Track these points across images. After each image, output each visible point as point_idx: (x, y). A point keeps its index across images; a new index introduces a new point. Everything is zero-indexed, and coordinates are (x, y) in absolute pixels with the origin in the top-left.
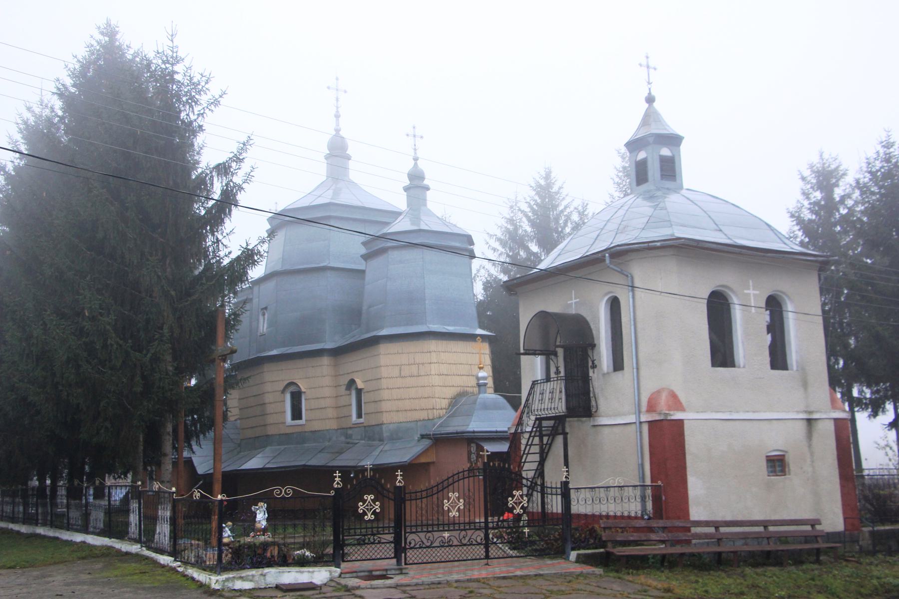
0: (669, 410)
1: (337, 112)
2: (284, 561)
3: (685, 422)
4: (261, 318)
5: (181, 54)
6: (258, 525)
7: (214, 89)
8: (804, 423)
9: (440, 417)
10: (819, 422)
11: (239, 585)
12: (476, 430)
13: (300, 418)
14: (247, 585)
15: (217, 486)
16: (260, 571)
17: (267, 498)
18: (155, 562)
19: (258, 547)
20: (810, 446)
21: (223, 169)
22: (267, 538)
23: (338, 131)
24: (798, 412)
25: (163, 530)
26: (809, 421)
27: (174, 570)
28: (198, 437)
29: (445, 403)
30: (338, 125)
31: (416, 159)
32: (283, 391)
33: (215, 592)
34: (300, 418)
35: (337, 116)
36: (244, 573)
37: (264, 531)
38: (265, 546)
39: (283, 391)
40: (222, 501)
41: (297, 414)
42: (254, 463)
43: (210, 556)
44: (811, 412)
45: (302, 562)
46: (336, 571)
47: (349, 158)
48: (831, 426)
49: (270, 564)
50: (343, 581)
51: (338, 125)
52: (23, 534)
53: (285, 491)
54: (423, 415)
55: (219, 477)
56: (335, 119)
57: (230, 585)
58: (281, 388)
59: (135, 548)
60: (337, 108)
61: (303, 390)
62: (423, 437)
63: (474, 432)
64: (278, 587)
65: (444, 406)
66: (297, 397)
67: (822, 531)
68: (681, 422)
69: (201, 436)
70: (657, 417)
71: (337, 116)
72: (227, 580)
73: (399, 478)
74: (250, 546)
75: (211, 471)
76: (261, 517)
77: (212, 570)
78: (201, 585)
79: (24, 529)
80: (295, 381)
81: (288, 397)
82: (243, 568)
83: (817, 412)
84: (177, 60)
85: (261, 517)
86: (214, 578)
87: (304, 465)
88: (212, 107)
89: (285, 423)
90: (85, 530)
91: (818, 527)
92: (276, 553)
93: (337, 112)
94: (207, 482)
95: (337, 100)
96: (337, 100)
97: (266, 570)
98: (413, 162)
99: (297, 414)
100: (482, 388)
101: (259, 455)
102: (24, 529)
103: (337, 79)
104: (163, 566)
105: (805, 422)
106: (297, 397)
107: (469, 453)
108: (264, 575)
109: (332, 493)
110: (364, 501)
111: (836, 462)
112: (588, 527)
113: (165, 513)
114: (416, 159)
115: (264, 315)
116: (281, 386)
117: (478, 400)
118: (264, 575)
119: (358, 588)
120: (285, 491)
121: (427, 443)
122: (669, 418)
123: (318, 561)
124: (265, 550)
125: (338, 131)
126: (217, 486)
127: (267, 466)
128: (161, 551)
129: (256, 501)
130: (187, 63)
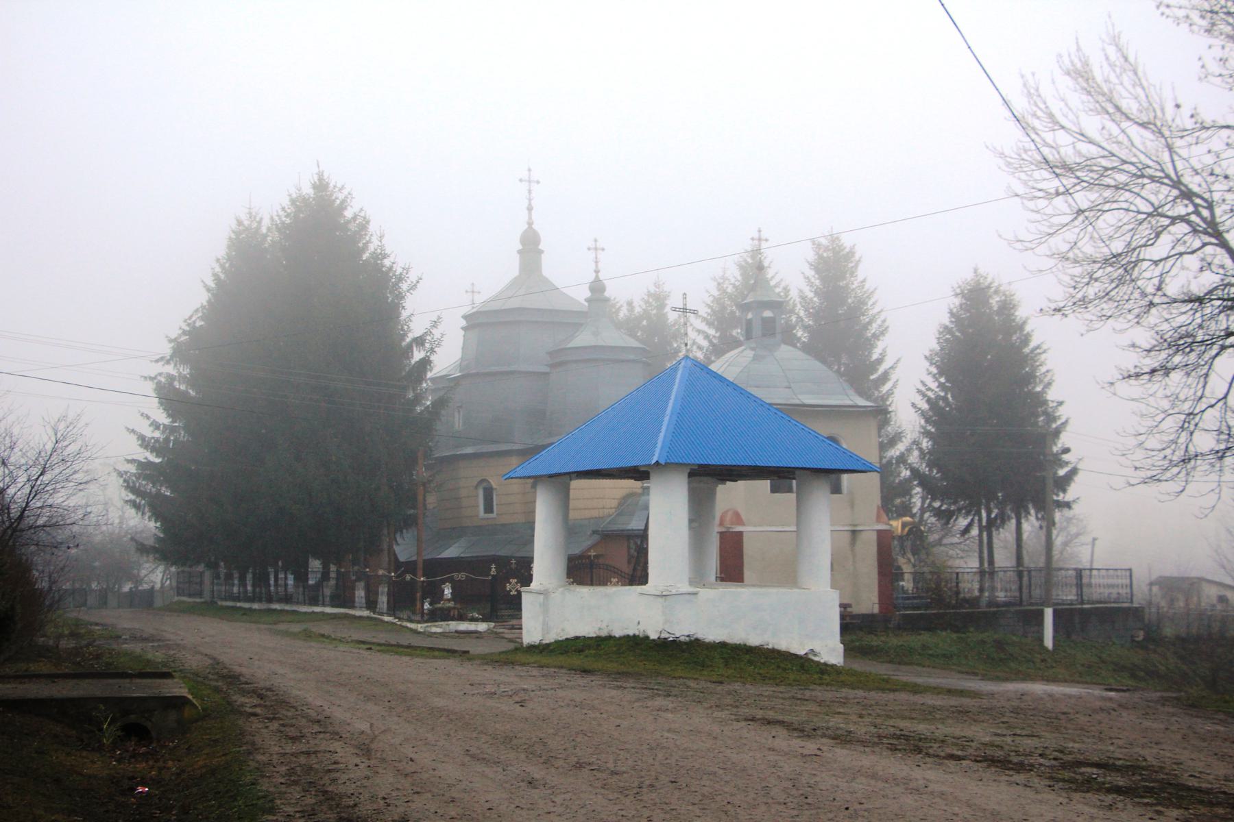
0: (732, 524)
1: (530, 204)
2: (461, 618)
3: (745, 534)
4: (456, 415)
5: (388, 251)
6: (445, 597)
7: (413, 277)
8: (849, 533)
9: (610, 516)
10: (863, 533)
11: (434, 630)
12: (634, 528)
13: (492, 511)
14: (439, 630)
15: (420, 572)
16: (446, 623)
17: (451, 580)
18: (382, 621)
19: (446, 610)
20: (852, 550)
21: (420, 341)
22: (451, 604)
23: (530, 224)
24: (843, 525)
25: (383, 600)
26: (854, 532)
27: (395, 624)
28: (402, 532)
29: (615, 503)
30: (530, 218)
31: (597, 272)
32: (476, 487)
33: (420, 633)
34: (492, 511)
35: (530, 209)
36: (437, 624)
37: (449, 600)
38: (449, 609)
39: (476, 487)
40: (423, 582)
41: (489, 508)
42: (452, 552)
43: (418, 618)
44: (856, 525)
45: (473, 620)
46: (492, 624)
47: (541, 252)
48: (874, 536)
49: (452, 619)
50: (495, 630)
51: (530, 218)
52: (255, 610)
53: (462, 576)
54: (595, 513)
55: (420, 565)
56: (527, 212)
57: (428, 629)
58: (475, 483)
59: (366, 613)
60: (530, 200)
61: (494, 486)
62: (595, 532)
63: (633, 530)
64: (457, 632)
65: (613, 506)
66: (489, 493)
67: (851, 612)
68: (741, 534)
69: (404, 531)
70: (724, 530)
71: (530, 209)
72: (427, 626)
73: (493, 569)
74: (441, 609)
75: (414, 558)
76: (448, 592)
77: (419, 622)
78: (411, 630)
79: (246, 605)
80: (487, 478)
81: (481, 493)
82: (436, 621)
83: (860, 525)
84: (385, 256)
85: (448, 592)
86: (419, 625)
87: (494, 555)
88: (411, 291)
89: (477, 516)
90: (324, 605)
91: (849, 610)
92: (456, 613)
93: (530, 204)
94: (410, 567)
95: (530, 192)
96: (530, 192)
97: (450, 622)
98: (594, 275)
99: (489, 508)
100: (646, 491)
101: (456, 545)
102: (246, 605)
103: (529, 170)
104: (387, 622)
105: (849, 533)
106: (489, 493)
107: (629, 548)
108: (448, 625)
109: (490, 578)
110: (510, 583)
111: (876, 564)
112: (959, 638)
113: (383, 589)
114: (597, 272)
115: (459, 412)
116: (475, 482)
117: (640, 502)
118: (448, 625)
119: (503, 633)
120: (462, 576)
121: (596, 538)
122: (731, 530)
123: (483, 620)
124: (450, 611)
125: (530, 224)
126: (420, 572)
127: (462, 555)
128: (382, 614)
129: (444, 582)
130: (391, 259)
